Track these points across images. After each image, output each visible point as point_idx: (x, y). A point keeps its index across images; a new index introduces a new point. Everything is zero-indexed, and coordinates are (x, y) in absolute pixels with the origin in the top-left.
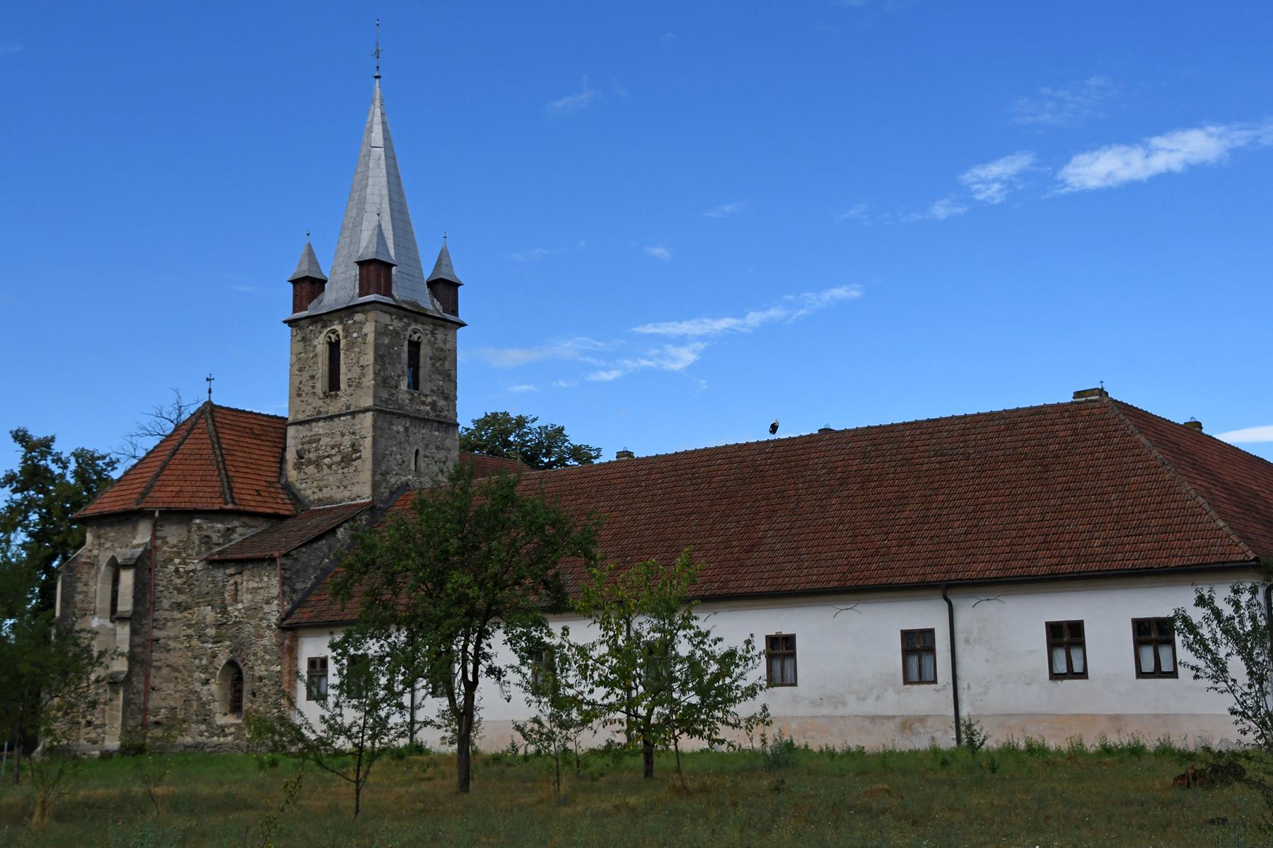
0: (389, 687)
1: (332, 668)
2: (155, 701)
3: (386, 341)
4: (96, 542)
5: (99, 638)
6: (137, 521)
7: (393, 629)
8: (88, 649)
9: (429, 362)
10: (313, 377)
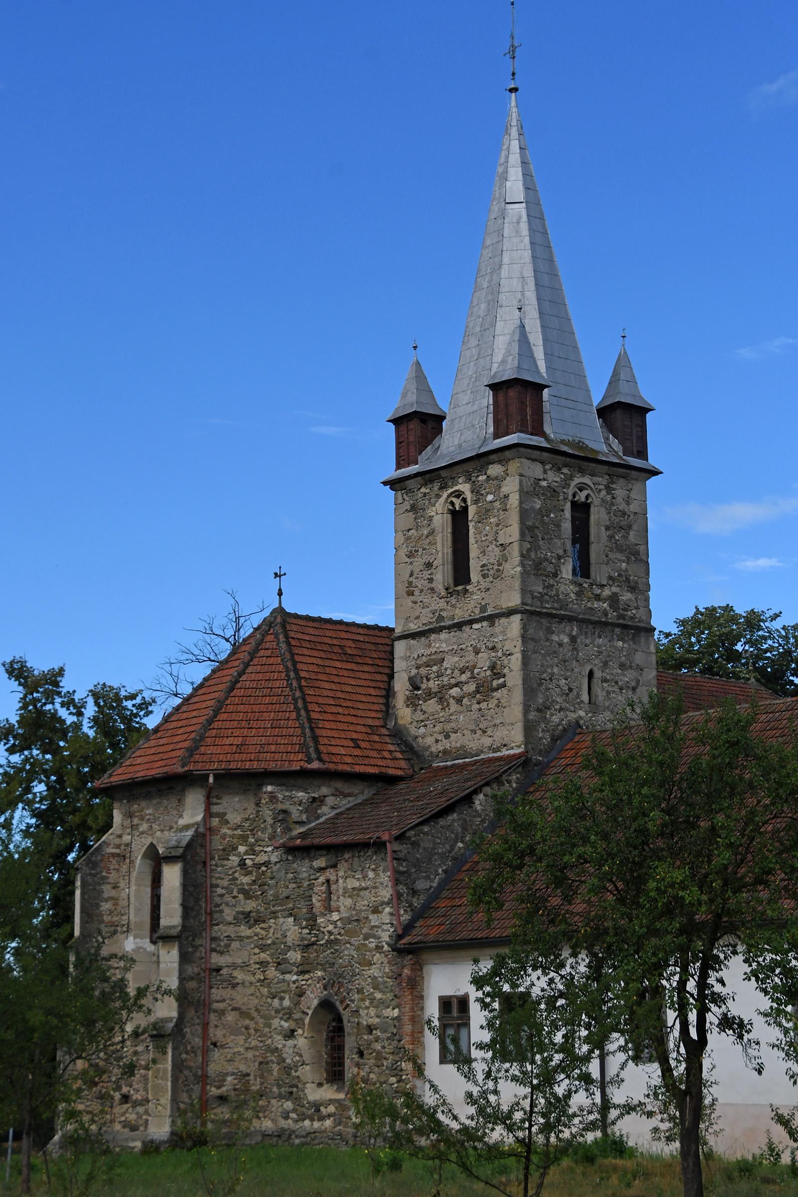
0: (567, 1048)
1: (477, 1016)
2: (217, 1063)
3: (538, 504)
4: (128, 822)
5: (137, 968)
6: (183, 791)
7: (566, 953)
8: (121, 984)
9: (604, 534)
10: (429, 565)
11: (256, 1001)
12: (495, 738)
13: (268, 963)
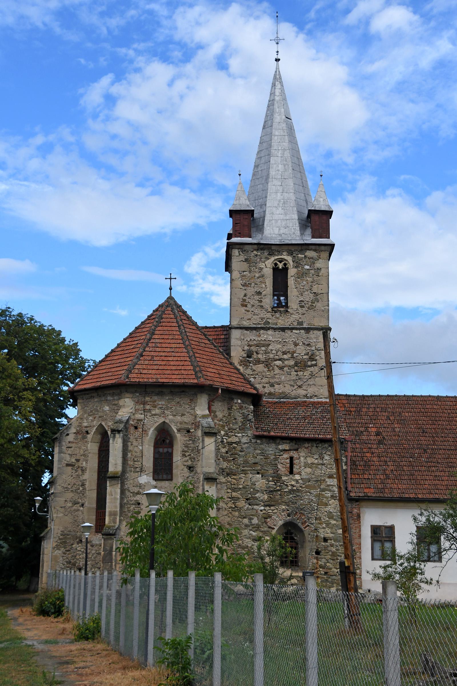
6: (196, 394)
11: (229, 519)
12: (308, 391)
13: (239, 498)
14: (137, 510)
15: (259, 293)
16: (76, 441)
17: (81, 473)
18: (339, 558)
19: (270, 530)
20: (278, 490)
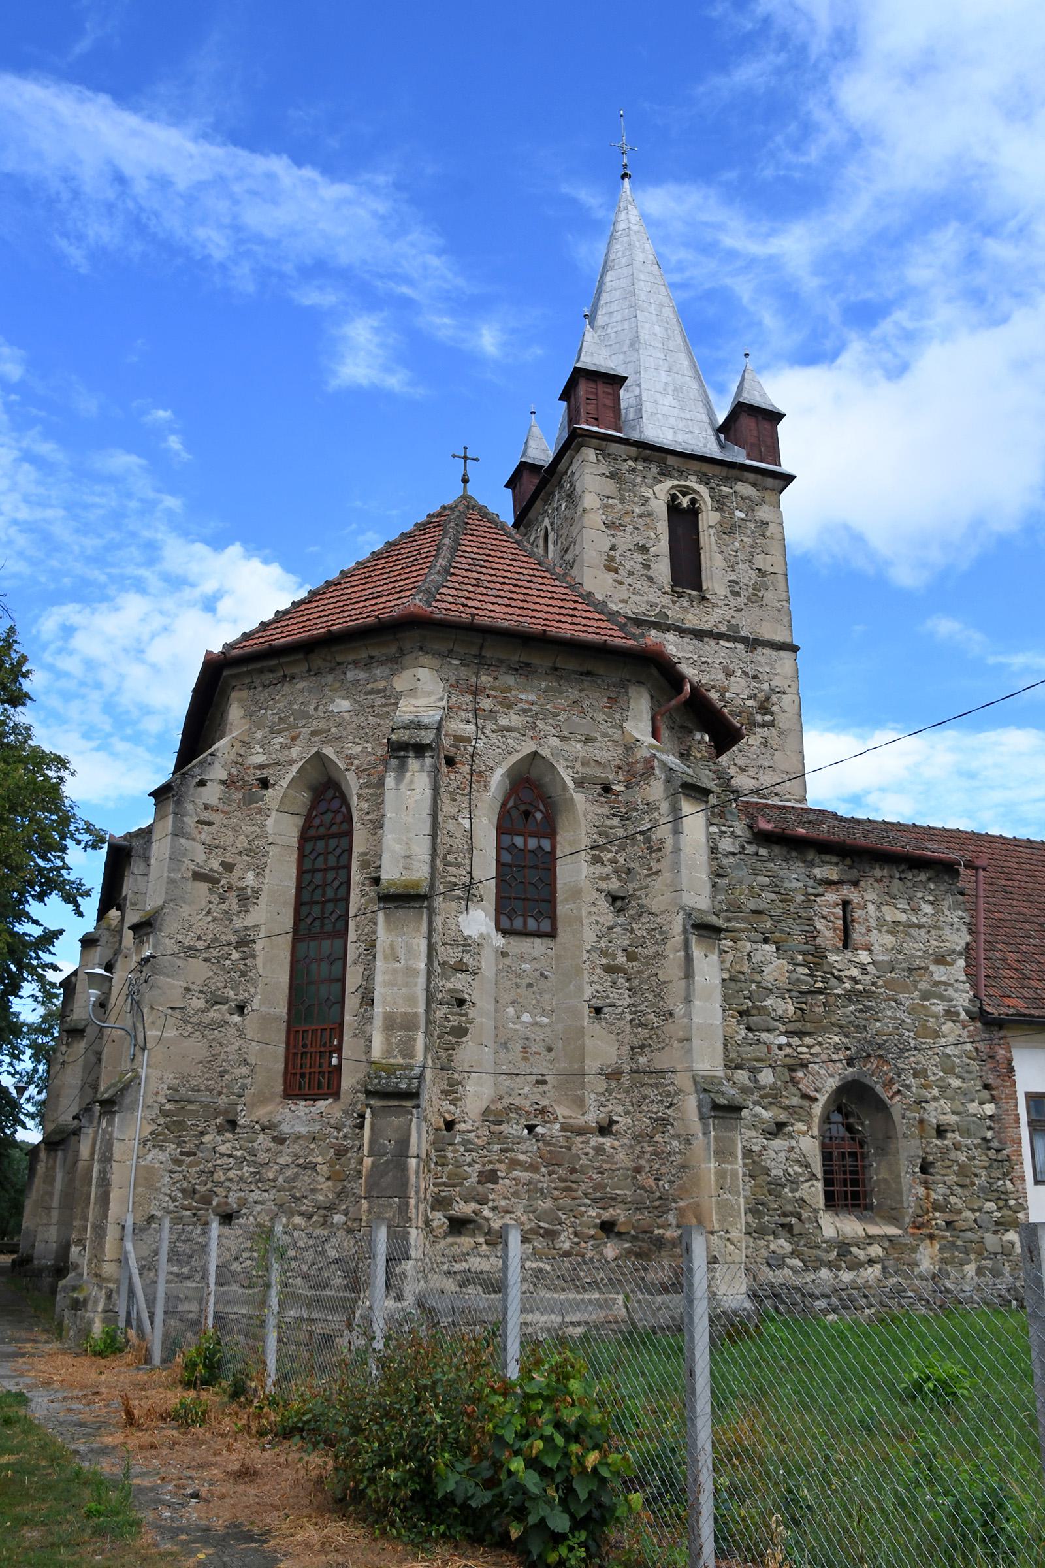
6: (623, 685)
12: (762, 780)
14: (455, 1021)
15: (643, 549)
16: (227, 808)
17: (235, 907)
18: (976, 1181)
19: (806, 1103)
20: (820, 992)
